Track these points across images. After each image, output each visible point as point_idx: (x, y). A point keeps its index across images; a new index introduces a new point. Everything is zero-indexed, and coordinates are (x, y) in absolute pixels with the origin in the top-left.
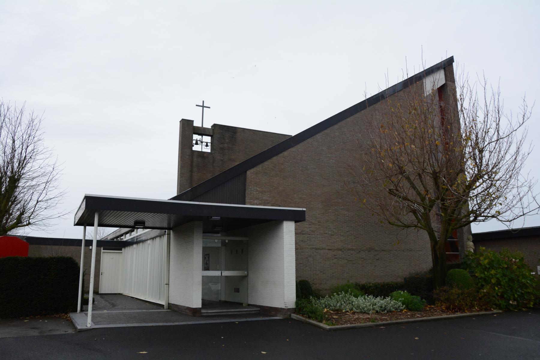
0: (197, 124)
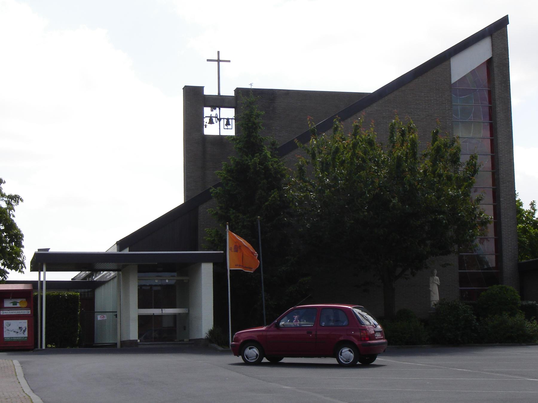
0: (210, 91)
